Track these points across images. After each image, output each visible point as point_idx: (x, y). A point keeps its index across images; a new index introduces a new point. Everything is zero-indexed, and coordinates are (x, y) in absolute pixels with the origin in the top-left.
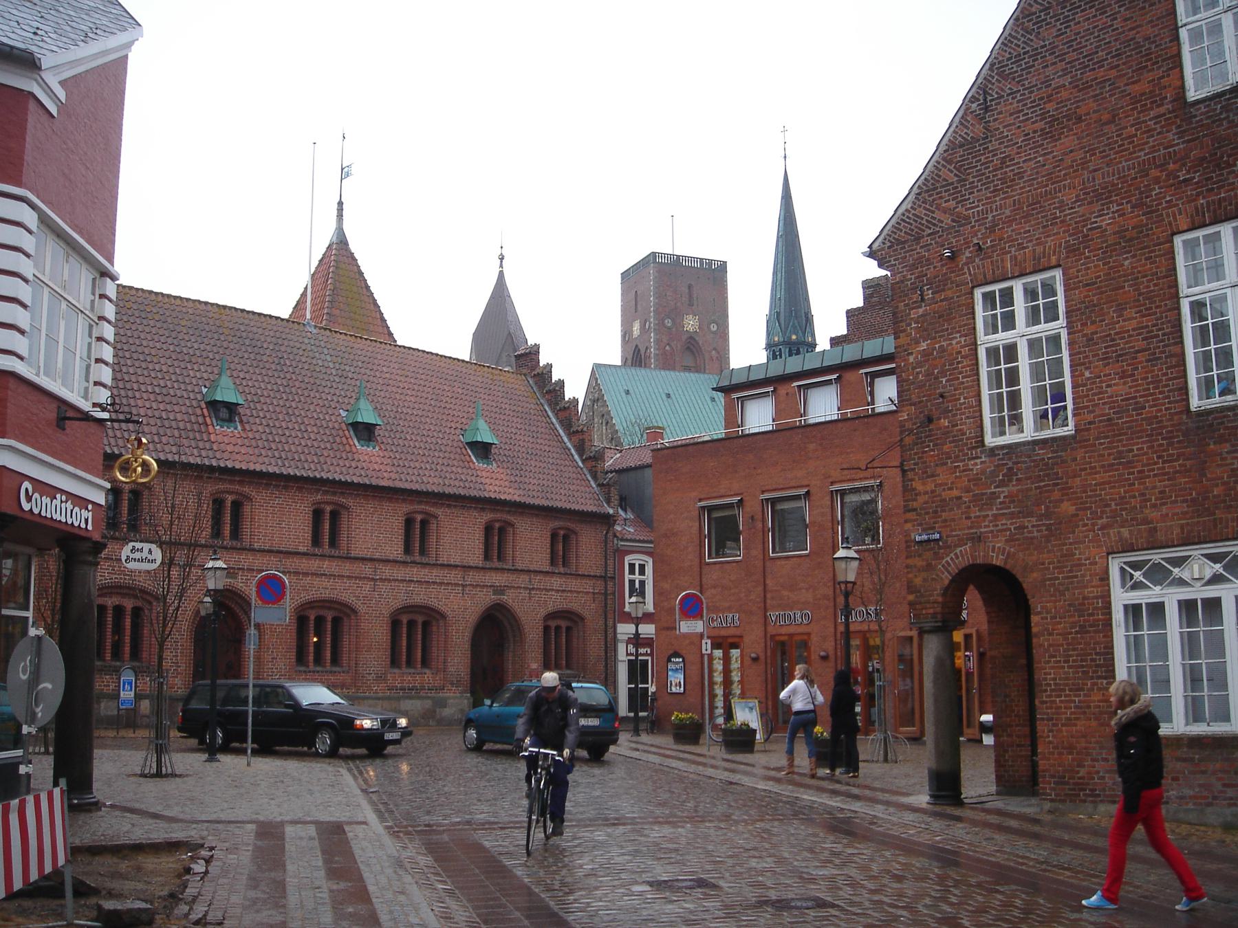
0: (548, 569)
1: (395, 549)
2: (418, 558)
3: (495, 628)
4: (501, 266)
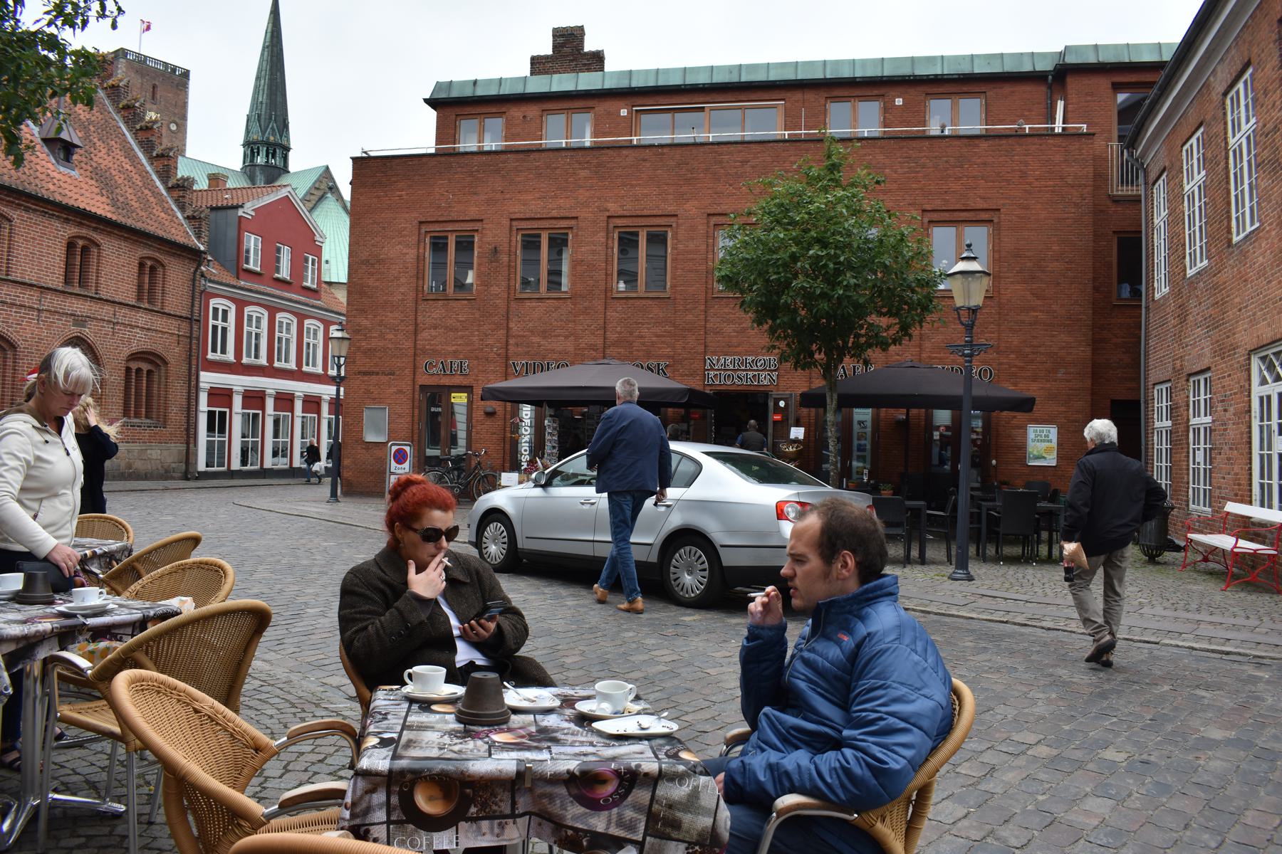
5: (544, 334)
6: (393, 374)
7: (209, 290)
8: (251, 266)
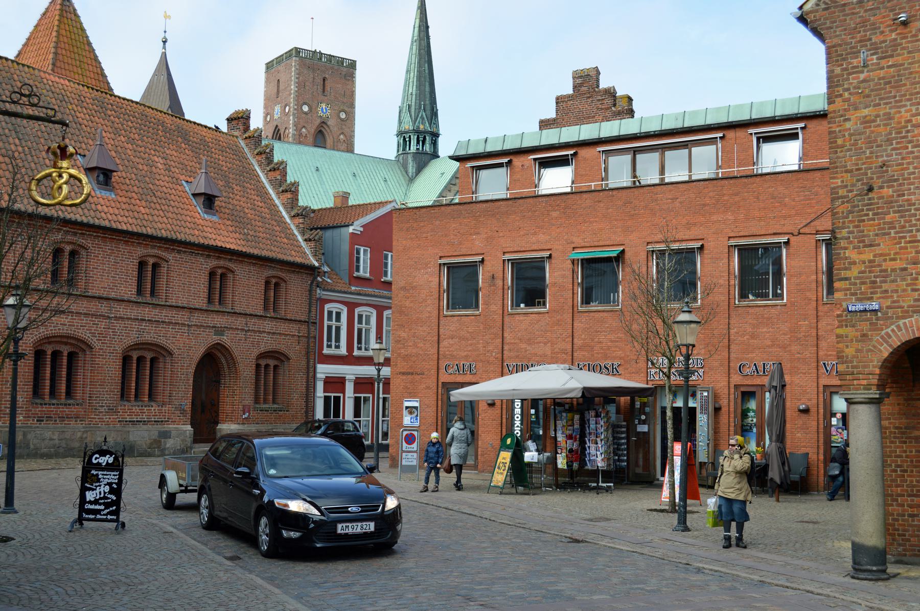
0: (261, 313)
1: (128, 290)
2: (148, 299)
3: (212, 366)
4: (164, 48)
5: (530, 342)
6: (423, 374)
7: (324, 297)
8: (361, 273)
